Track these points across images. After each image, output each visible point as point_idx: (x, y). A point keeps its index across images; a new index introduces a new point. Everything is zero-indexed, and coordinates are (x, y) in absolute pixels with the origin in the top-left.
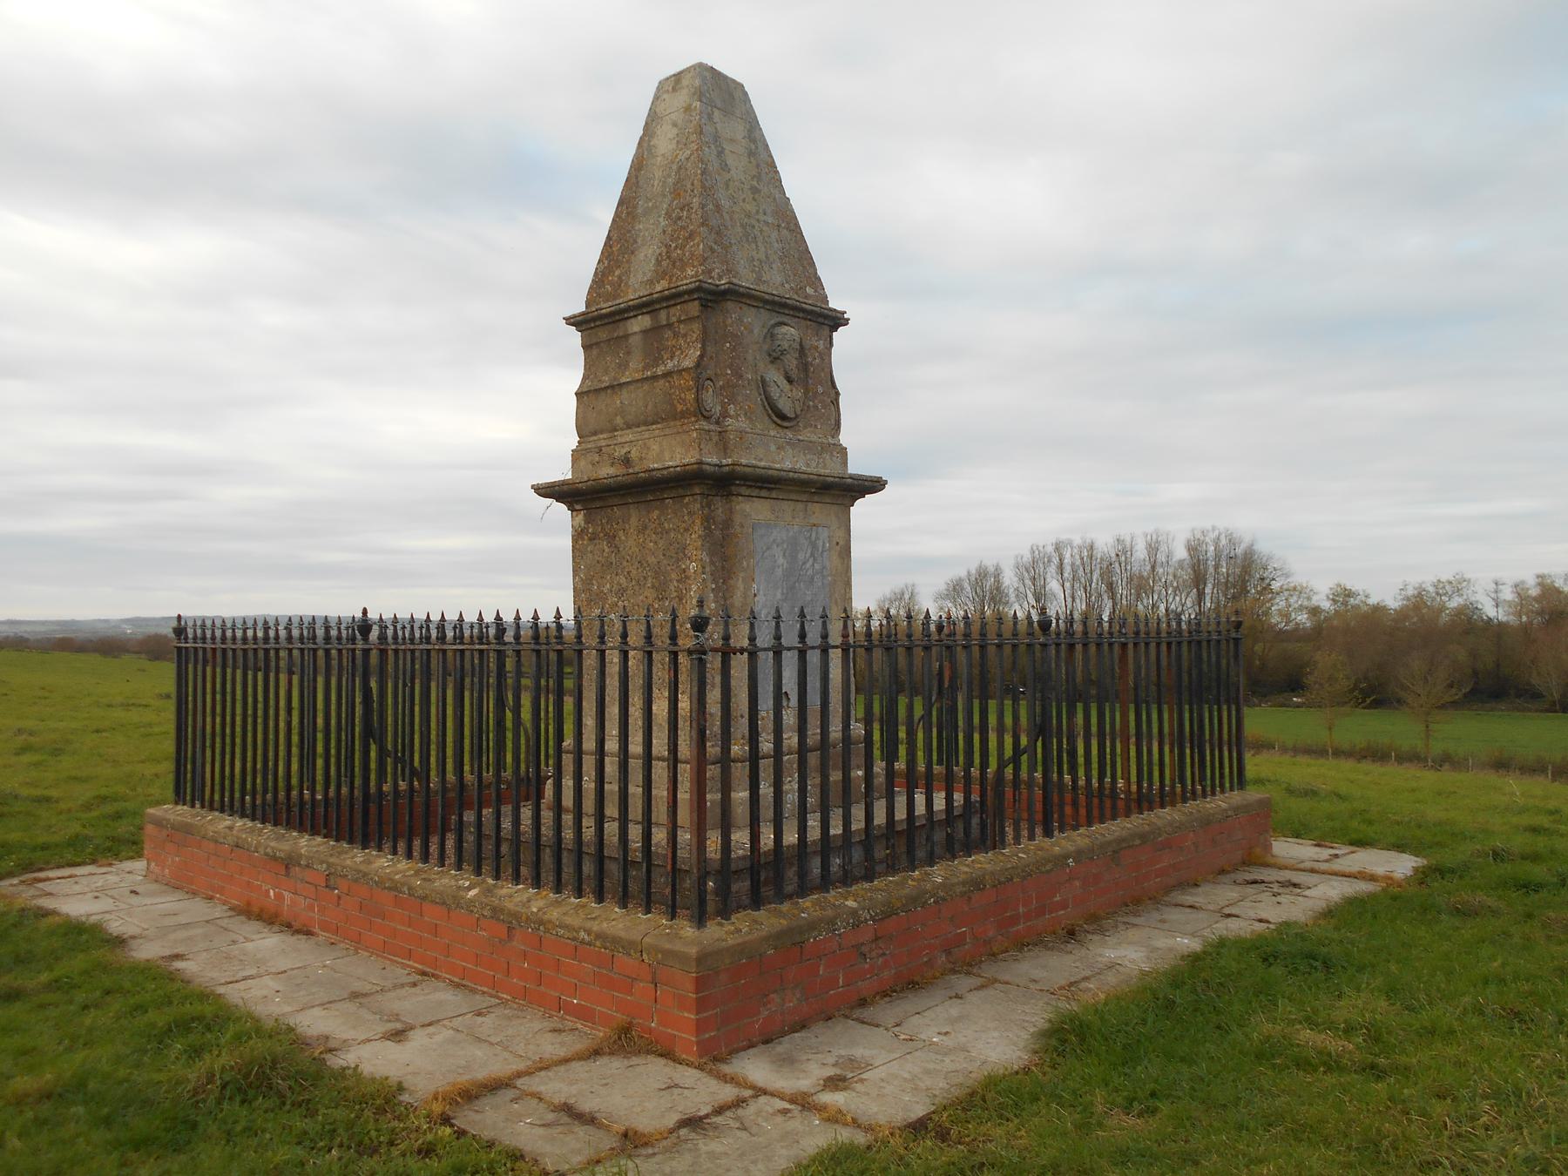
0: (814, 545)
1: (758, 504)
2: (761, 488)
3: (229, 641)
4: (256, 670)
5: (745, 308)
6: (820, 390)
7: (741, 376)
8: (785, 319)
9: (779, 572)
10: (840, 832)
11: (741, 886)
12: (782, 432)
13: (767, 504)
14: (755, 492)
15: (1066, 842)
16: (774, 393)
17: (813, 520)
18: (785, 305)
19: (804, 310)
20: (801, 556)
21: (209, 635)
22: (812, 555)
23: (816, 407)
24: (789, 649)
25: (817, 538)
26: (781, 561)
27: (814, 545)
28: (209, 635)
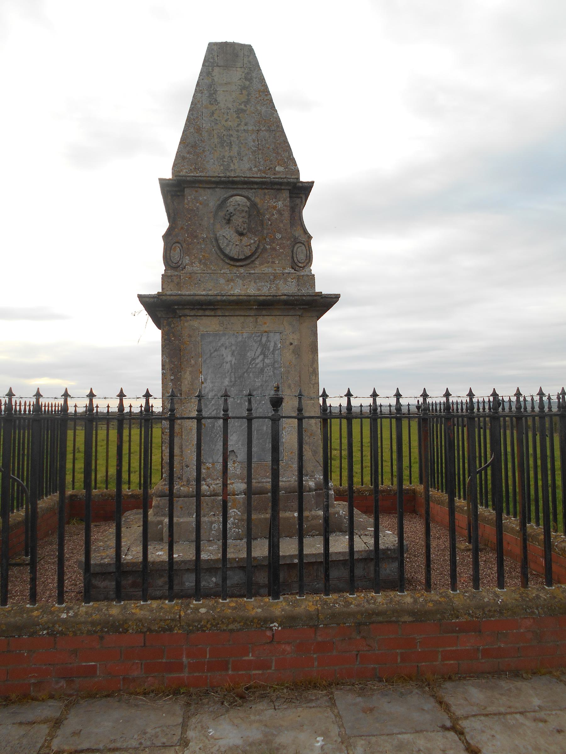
0: (265, 347)
1: (205, 320)
2: (205, 310)
3: (460, 410)
4: (463, 426)
5: (201, 191)
6: (278, 236)
7: (196, 237)
8: (235, 192)
9: (227, 367)
10: (266, 553)
11: (262, 578)
12: (235, 270)
13: (215, 320)
14: (200, 313)
15: (281, 606)
16: (223, 243)
17: (265, 328)
18: (233, 182)
19: (256, 183)
20: (250, 355)
21: (438, 409)
22: (262, 353)
23: (274, 249)
24: (356, 418)
25: (268, 341)
26: (229, 358)
27: (265, 347)
28: (438, 409)
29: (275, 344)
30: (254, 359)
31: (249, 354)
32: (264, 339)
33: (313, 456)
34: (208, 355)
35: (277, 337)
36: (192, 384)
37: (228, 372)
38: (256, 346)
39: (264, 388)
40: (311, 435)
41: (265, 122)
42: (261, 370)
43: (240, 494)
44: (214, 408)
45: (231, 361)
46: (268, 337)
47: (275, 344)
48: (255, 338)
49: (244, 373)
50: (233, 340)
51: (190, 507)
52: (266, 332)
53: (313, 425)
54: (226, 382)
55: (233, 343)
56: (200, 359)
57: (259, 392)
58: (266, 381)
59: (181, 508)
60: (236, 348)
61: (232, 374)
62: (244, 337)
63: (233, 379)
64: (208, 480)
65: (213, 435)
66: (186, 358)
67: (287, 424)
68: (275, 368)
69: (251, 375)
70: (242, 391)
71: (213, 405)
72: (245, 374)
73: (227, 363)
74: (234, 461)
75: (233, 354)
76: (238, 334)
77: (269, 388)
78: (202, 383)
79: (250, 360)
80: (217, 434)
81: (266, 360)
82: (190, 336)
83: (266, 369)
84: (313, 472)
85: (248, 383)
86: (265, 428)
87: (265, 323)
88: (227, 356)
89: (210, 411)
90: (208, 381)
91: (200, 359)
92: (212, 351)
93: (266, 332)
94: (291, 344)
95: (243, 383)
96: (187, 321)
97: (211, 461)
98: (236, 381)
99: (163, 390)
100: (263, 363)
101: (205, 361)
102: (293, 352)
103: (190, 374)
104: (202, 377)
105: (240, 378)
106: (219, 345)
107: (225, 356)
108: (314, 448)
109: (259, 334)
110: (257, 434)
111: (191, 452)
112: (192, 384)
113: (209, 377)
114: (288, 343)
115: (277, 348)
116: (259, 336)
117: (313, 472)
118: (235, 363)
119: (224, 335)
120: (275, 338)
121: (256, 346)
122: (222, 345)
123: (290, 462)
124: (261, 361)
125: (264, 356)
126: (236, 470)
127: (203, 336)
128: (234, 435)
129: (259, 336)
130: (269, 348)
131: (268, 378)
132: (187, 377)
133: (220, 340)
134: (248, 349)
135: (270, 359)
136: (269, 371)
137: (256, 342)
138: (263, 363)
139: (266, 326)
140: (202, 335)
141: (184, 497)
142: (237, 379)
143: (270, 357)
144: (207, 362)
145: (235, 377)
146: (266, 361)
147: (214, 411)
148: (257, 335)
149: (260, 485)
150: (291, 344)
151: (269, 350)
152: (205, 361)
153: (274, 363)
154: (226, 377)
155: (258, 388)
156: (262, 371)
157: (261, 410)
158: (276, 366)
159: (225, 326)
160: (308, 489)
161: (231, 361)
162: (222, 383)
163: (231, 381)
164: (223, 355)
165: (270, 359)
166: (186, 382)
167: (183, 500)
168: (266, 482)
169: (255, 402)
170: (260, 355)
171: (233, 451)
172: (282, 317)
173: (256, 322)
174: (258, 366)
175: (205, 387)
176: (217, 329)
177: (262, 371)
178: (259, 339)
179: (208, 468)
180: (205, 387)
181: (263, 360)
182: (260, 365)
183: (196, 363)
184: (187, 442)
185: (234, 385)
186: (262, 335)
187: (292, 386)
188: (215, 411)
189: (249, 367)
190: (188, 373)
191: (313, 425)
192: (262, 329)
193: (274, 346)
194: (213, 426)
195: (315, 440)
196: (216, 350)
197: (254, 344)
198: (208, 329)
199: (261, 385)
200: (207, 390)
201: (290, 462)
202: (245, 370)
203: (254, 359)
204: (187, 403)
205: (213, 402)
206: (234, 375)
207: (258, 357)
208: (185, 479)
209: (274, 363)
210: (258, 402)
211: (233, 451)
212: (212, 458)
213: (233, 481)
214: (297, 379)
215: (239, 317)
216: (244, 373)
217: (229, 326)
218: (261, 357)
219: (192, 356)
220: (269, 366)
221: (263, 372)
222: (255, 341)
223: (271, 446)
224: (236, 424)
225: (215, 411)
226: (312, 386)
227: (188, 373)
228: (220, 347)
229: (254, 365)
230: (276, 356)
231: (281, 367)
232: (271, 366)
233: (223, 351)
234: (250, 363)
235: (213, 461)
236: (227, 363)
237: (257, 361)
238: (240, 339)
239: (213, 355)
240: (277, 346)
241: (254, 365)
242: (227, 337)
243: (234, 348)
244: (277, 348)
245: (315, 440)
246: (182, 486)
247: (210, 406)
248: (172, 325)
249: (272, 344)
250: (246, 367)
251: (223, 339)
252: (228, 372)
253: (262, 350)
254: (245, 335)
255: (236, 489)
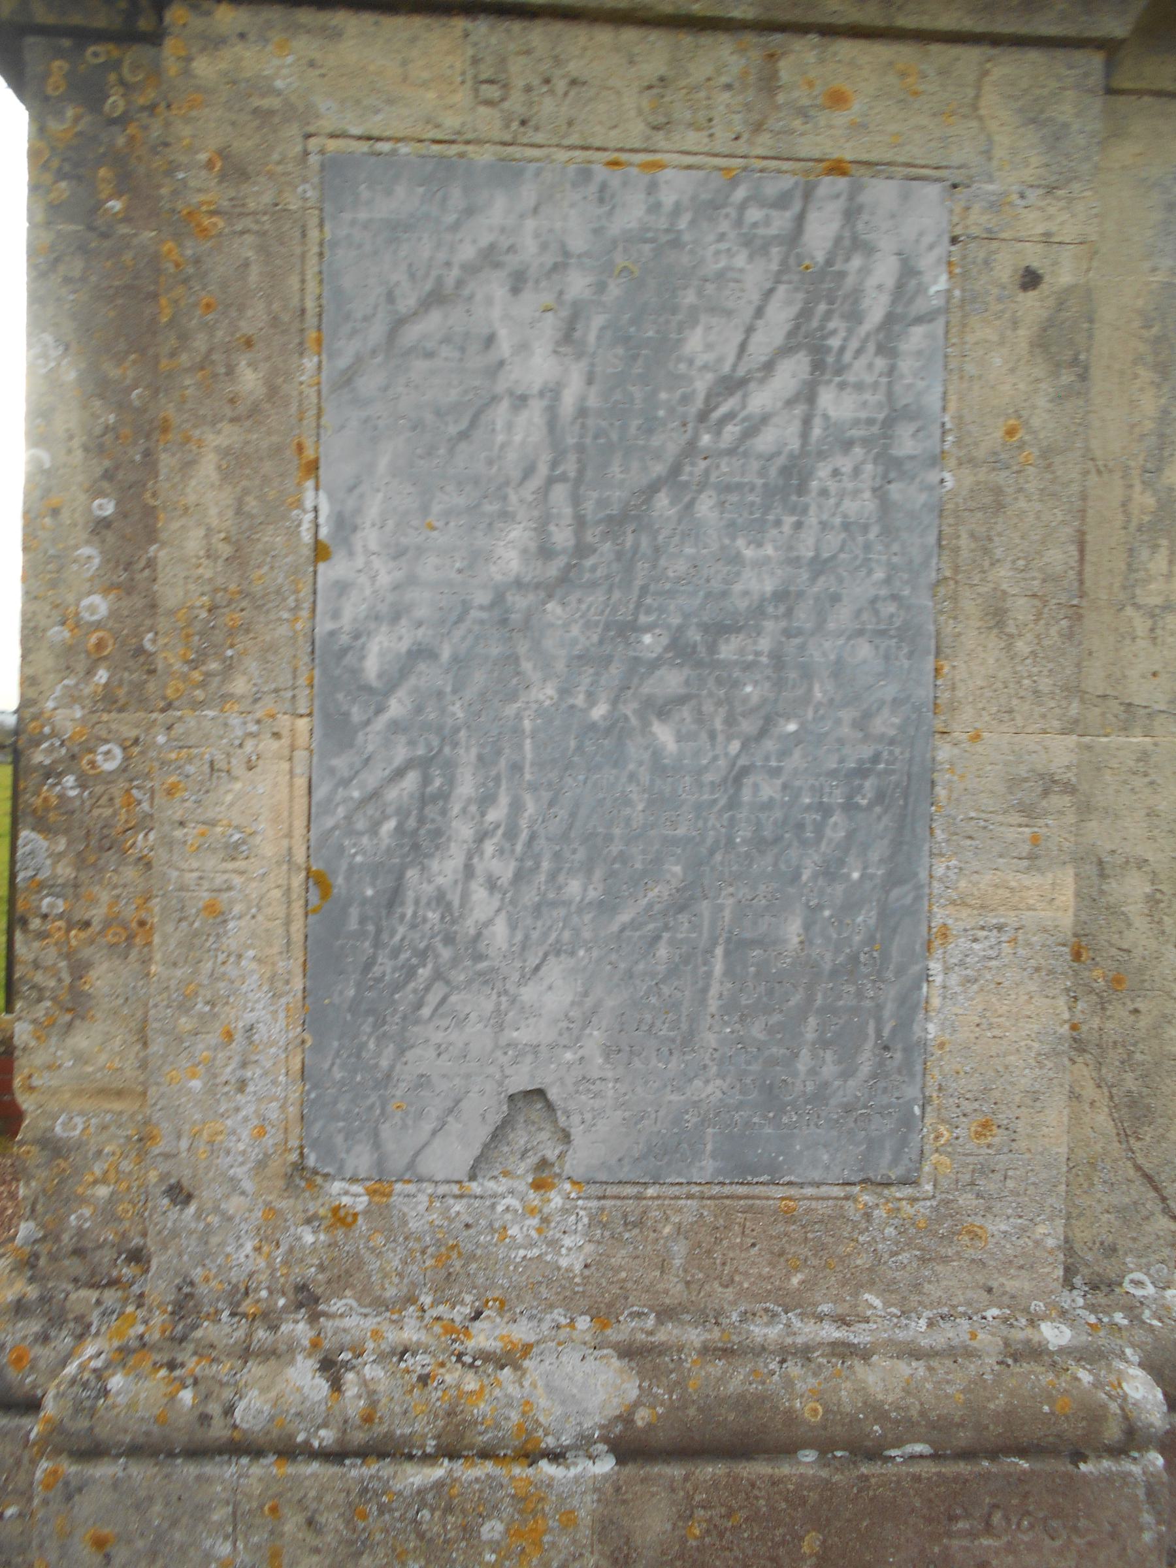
0: (823, 287)
9: (522, 432)
17: (827, 138)
20: (706, 347)
22: (806, 339)
25: (853, 242)
26: (539, 366)
27: (823, 287)
29: (908, 270)
30: (731, 385)
31: (694, 342)
32: (822, 231)
33: (1123, 1136)
34: (377, 332)
35: (927, 214)
36: (239, 559)
37: (529, 472)
38: (755, 274)
39: (803, 616)
40: (1116, 982)
41: (480, 1515)
42: (786, 471)
43: (584, 1445)
44: (401, 753)
45: (552, 393)
46: (851, 213)
47: (908, 270)
48: (754, 214)
49: (653, 489)
50: (574, 223)
51: (178, 1536)
52: (837, 168)
53: (1135, 909)
54: (509, 554)
55: (578, 243)
56: (310, 363)
57: (764, 644)
58: (819, 566)
59: (100, 1543)
60: (601, 287)
61: (560, 493)
62: (668, 199)
63: (562, 537)
64: (336, 1306)
65: (385, 966)
66: (200, 343)
67: (961, 902)
68: (892, 467)
69: (705, 507)
70: (627, 630)
71: (395, 727)
72: (662, 500)
73: (521, 401)
74: (544, 1164)
75: (568, 337)
76: (615, 179)
77: (842, 617)
78: (320, 552)
79: (702, 385)
80: (423, 955)
81: (827, 398)
82: (233, 170)
83: (823, 471)
84: (1111, 1250)
85: (679, 567)
86: (793, 929)
87: (837, 99)
88: (523, 348)
89: (372, 778)
90: (369, 537)
91: (310, 363)
92: (408, 301)
93: (837, 168)
94: (1031, 279)
95: (642, 569)
96: (214, 43)
97: (361, 1160)
98: (581, 550)
99: (30, 596)
100: (807, 422)
101: (347, 379)
102: (1042, 343)
103: (226, 475)
104: (317, 505)
105: (615, 524)
106: (467, 253)
107: (505, 346)
108: (1130, 1081)
109: (786, 182)
110: (729, 972)
111: (210, 1090)
112: (239, 559)
113: (374, 509)
114: (1005, 268)
115: (920, 306)
116: (782, 202)
117: (1111, 1250)
118: (582, 412)
119: (507, 174)
120: (913, 221)
121: (755, 274)
122: (490, 257)
123: (966, 1200)
124: (790, 403)
125: (818, 366)
126: (554, 1244)
127: (335, 170)
128: (554, 970)
129: (782, 202)
130: (857, 294)
131: (834, 540)
132: (202, 497)
133: (469, 211)
134: (689, 298)
135: (859, 387)
136: (845, 489)
137: (756, 246)
138: (807, 422)
139: (840, 118)
140: (333, 166)
141: (135, 1451)
142: (591, 536)
143: (858, 371)
144: (369, 383)
145: (580, 523)
146: (834, 404)
147: (400, 773)
148: (772, 188)
149: (737, 1380)
150: (1031, 279)
151: (855, 317)
152: (347, 379)
153: (889, 423)
154: (506, 516)
155: (759, 611)
156: (793, 478)
157: (769, 790)
158: (906, 444)
159: (516, 103)
160: (1113, 1432)
161: (552, 393)
162: (477, 558)
163: (546, 552)
164: (490, 340)
165: (859, 387)
166: (194, 543)
167: (116, 1484)
168: (785, 1353)
169: (730, 721)
170: (786, 350)
171: (540, 1093)
172: (971, 55)
173: (769, 83)
174: (765, 441)
175: (342, 588)
176: (452, 122)
177: (793, 478)
178: (781, 221)
179: (341, 1218)
180: (342, 588)
181: (808, 394)
182: (782, 434)
183: (273, 391)
184: (184, 1006)
185: (564, 579)
186: (808, 194)
187: (1021, 609)
188: (411, 780)
189: (691, 449)
190: (208, 467)
191: (1135, 909)
192: (808, 146)
193: (900, 287)
194: (394, 897)
195: (1144, 1022)
196: (436, 298)
197: (740, 260)
198: (374, 124)
199: (781, 596)
200: (352, 610)
201: (966, 1200)
202: (659, 469)
203: (731, 385)
204: (197, 705)
205: (396, 707)
206: (576, 500)
207: (769, 367)
208: (158, 1287)
209: (889, 423)
210: (748, 726)
211: (540, 1093)
212: (377, 1145)
213: (522, 1332)
214: (1059, 557)
215: (630, 35)
216: (653, 489)
217: (548, 105)
218: (791, 373)
219: (246, 328)
220: (847, 445)
221: (802, 490)
222: (747, 241)
223: (1160, 1396)
224: (574, 887)
225: (411, 780)
226: (1141, 625)
227: (208, 467)
228: (471, 269)
229: (731, 431)
230: (905, 366)
231: (937, 460)
232: (866, 442)
233: (492, 304)
234: (703, 417)
235: (380, 1164)
236: (521, 401)
237: (760, 399)
238: (632, 213)
239: (412, 333)
240: (921, 290)
241: (731, 431)
242: (528, 194)
243: (578, 284)
244: (920, 306)
245: (1144, 1022)
246: (124, 1355)
247: (370, 739)
248: (115, 102)
249: (885, 271)
250: (670, 442)
251: (498, 211)
252: (529, 472)
253: (805, 314)
254: (676, 186)
255: (548, 1410)
